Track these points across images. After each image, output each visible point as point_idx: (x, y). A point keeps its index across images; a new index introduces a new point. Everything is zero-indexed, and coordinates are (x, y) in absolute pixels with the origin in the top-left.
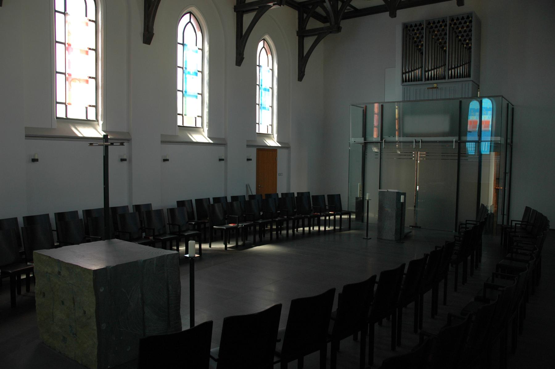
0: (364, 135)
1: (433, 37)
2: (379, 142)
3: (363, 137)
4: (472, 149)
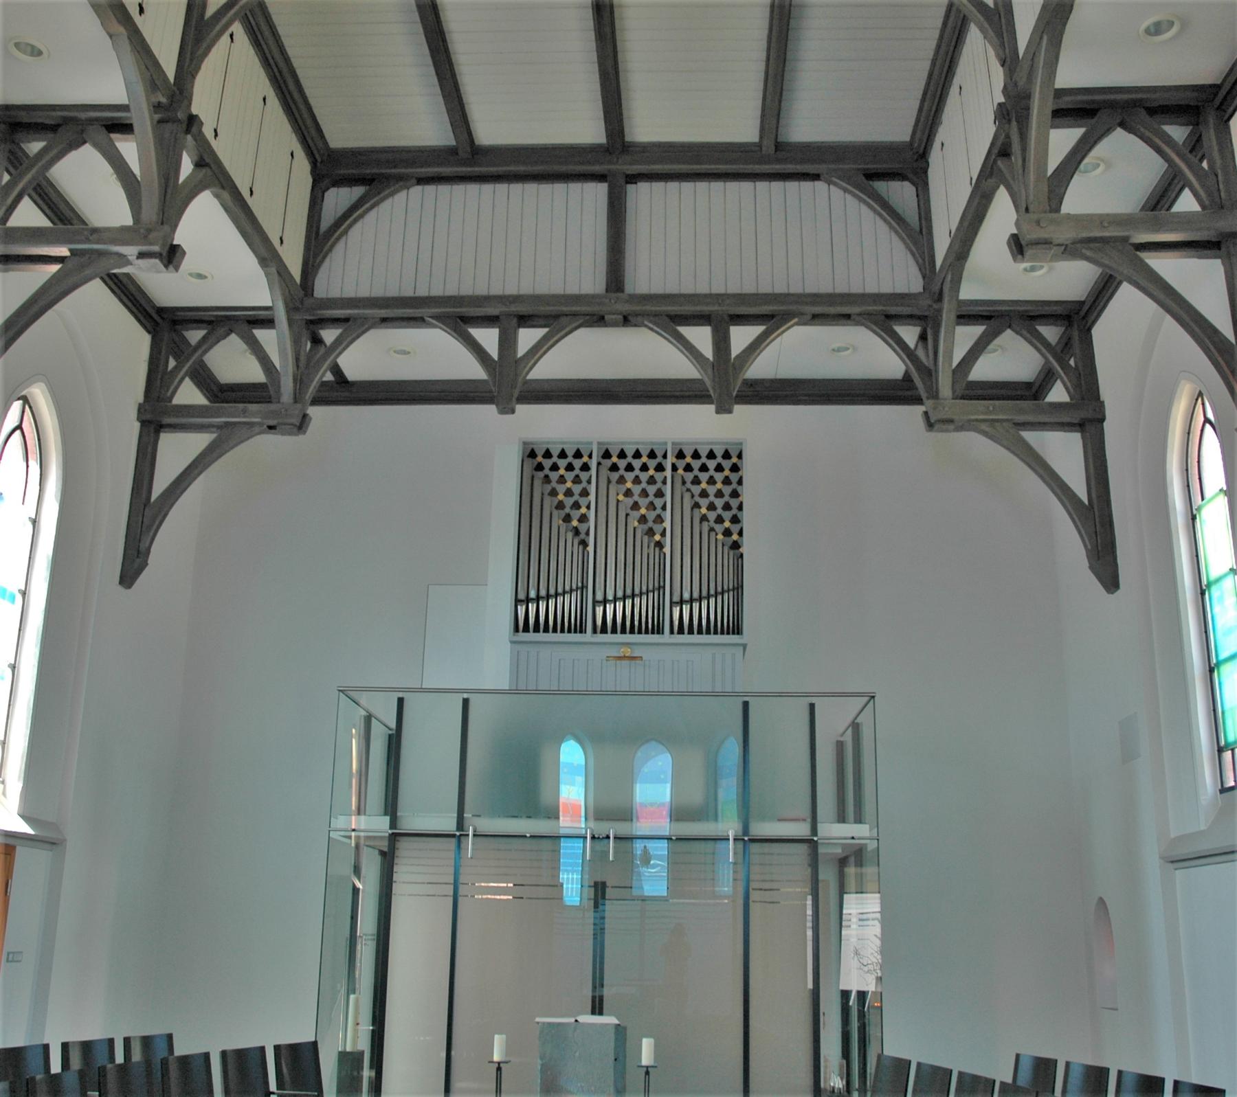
0: (391, 807)
1: (621, 497)
2: (454, 836)
3: (386, 814)
4: (575, 886)
